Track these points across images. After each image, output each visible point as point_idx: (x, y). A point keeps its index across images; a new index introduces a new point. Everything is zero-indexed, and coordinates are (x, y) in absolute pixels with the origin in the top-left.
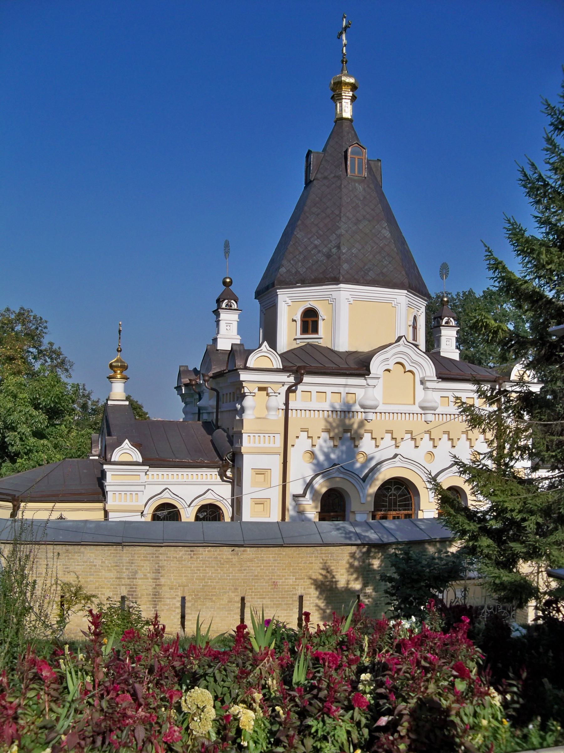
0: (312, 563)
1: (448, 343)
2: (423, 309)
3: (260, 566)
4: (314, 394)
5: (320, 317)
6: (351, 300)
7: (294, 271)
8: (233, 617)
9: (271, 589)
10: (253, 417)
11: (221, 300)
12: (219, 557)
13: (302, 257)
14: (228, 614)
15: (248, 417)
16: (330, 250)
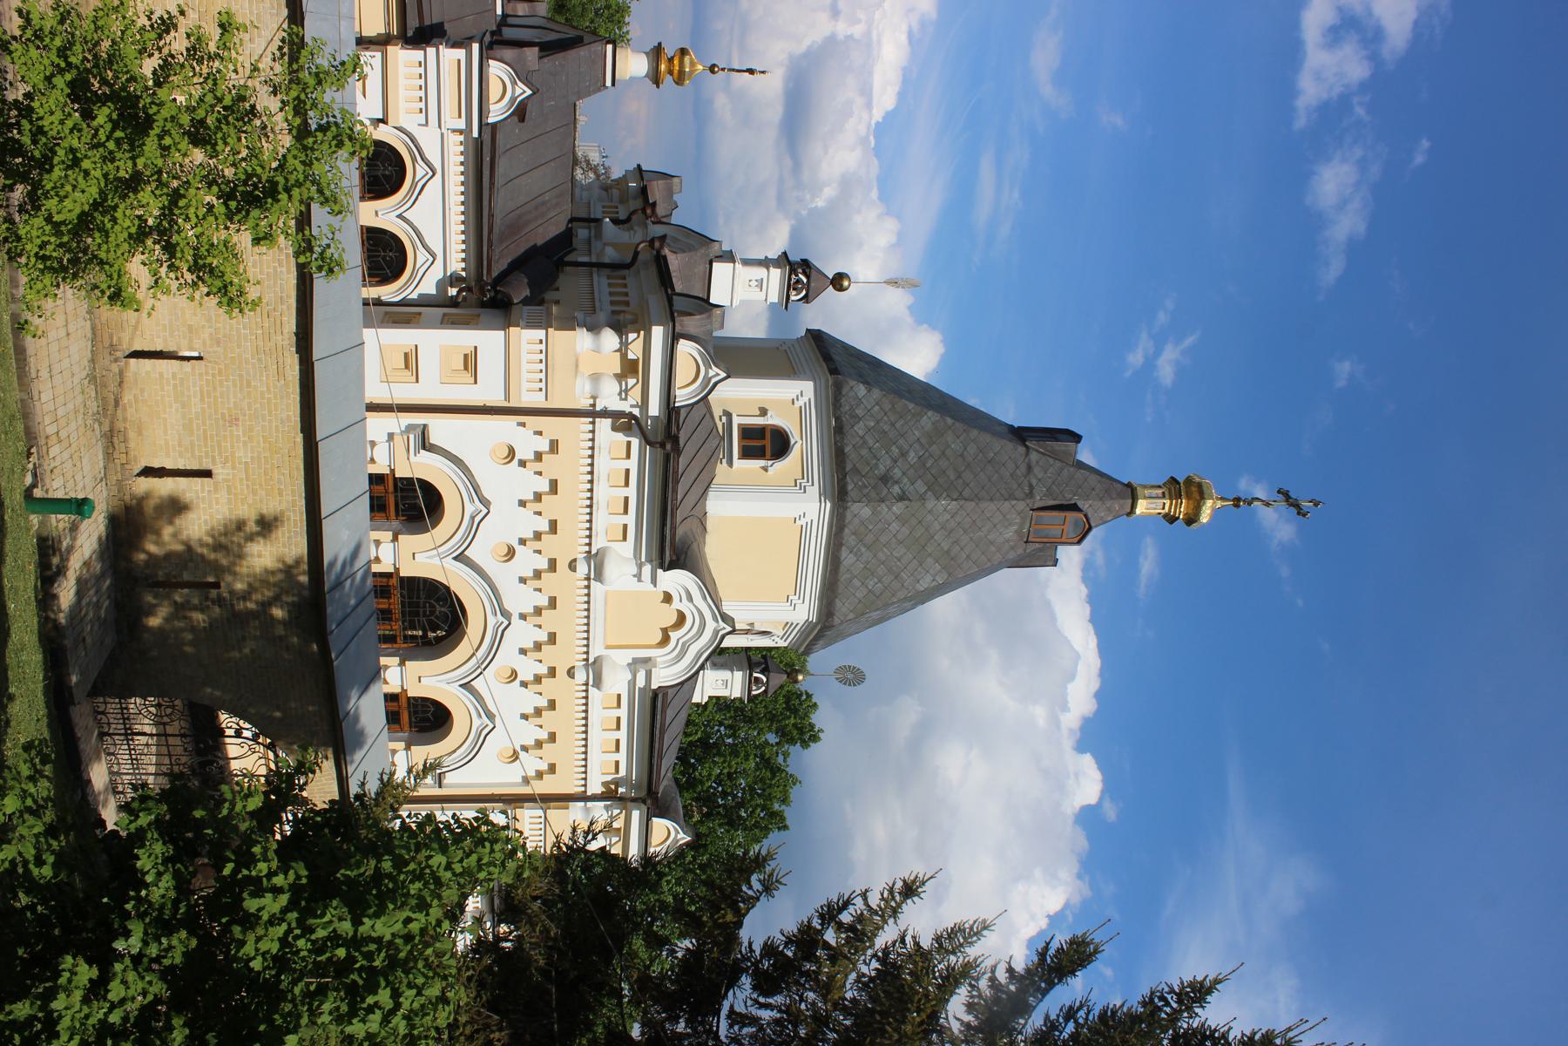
0: (280, 494)
1: (720, 682)
2: (782, 644)
3: (268, 390)
5: (770, 462)
7: (860, 412)
8: (158, 337)
9: (223, 414)
10: (578, 349)
11: (807, 271)
12: (285, 307)
13: (886, 428)
14: (165, 326)
15: (581, 339)
16: (897, 482)
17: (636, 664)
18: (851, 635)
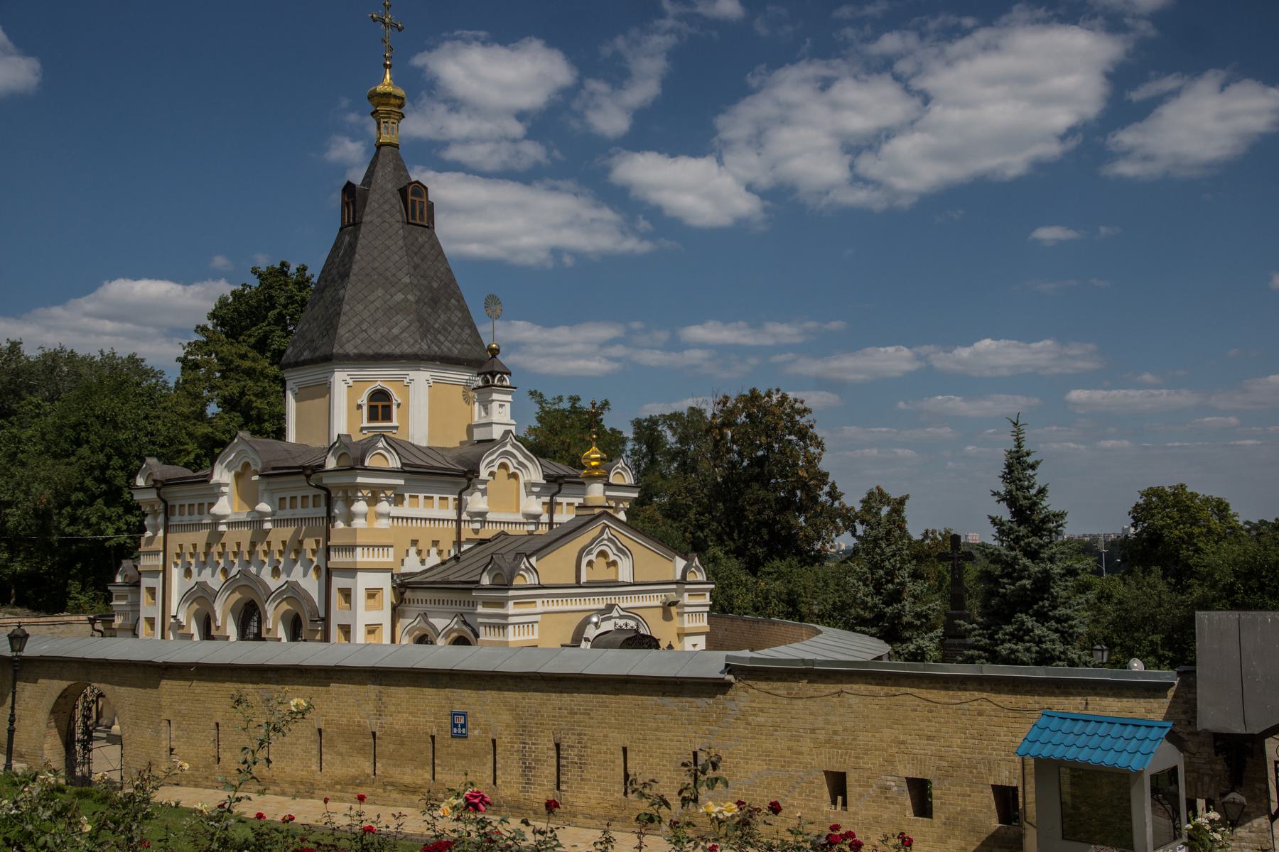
4: (564, 505)
5: (394, 401)
6: (431, 381)
17: (529, 493)
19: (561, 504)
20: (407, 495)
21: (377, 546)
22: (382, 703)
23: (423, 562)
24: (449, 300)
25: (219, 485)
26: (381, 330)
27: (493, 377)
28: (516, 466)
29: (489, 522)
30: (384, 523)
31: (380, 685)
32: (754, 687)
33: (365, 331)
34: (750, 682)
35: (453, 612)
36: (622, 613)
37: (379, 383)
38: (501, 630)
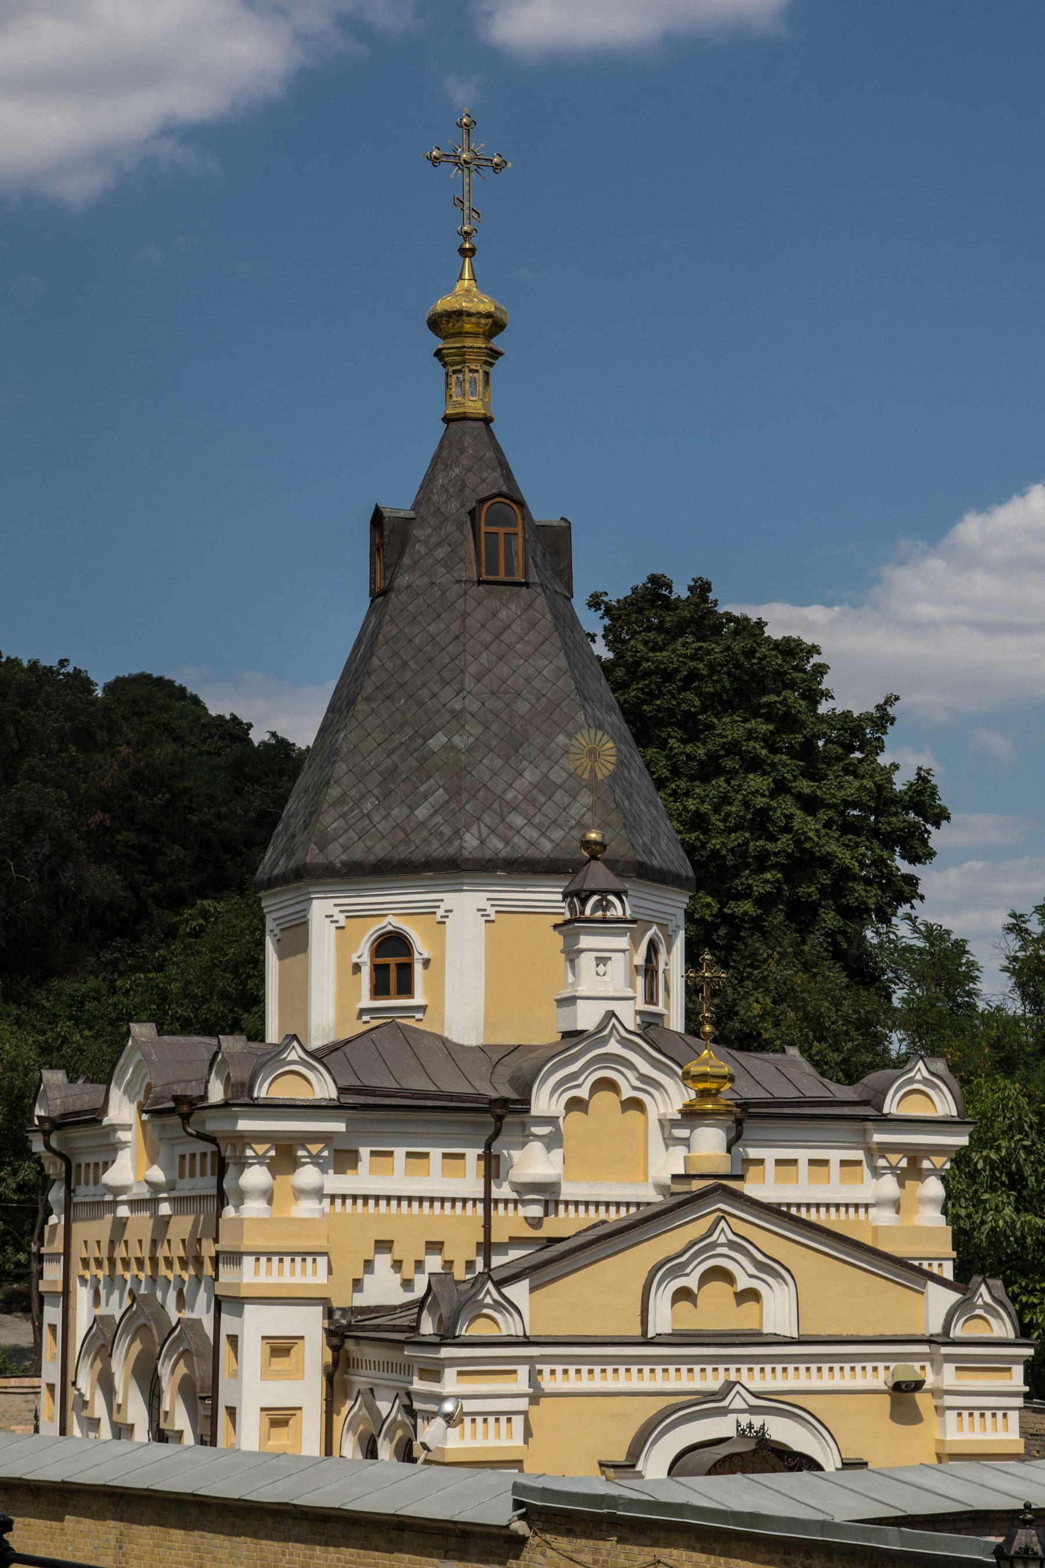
5: (416, 956)
6: (491, 911)
18: (372, 564)
19: (761, 1162)
20: (364, 1152)
21: (299, 1254)
22: (124, 1555)
23: (407, 1284)
24: (551, 738)
25: (114, 1128)
26: (396, 812)
27: (584, 902)
28: (638, 1084)
29: (567, 1203)
30: (307, 1208)
31: (121, 1520)
32: (553, 1545)
33: (368, 815)
34: (548, 1537)
35: (394, 1388)
36: (754, 1402)
37: (390, 919)
38: (426, 1422)
